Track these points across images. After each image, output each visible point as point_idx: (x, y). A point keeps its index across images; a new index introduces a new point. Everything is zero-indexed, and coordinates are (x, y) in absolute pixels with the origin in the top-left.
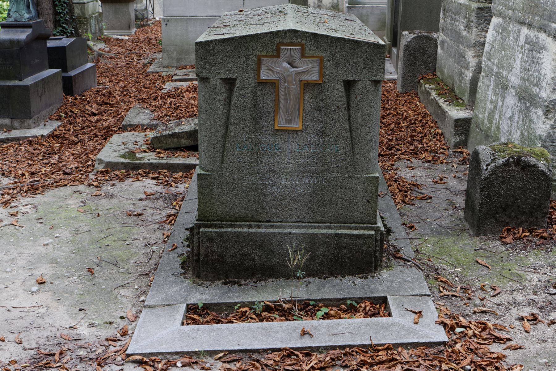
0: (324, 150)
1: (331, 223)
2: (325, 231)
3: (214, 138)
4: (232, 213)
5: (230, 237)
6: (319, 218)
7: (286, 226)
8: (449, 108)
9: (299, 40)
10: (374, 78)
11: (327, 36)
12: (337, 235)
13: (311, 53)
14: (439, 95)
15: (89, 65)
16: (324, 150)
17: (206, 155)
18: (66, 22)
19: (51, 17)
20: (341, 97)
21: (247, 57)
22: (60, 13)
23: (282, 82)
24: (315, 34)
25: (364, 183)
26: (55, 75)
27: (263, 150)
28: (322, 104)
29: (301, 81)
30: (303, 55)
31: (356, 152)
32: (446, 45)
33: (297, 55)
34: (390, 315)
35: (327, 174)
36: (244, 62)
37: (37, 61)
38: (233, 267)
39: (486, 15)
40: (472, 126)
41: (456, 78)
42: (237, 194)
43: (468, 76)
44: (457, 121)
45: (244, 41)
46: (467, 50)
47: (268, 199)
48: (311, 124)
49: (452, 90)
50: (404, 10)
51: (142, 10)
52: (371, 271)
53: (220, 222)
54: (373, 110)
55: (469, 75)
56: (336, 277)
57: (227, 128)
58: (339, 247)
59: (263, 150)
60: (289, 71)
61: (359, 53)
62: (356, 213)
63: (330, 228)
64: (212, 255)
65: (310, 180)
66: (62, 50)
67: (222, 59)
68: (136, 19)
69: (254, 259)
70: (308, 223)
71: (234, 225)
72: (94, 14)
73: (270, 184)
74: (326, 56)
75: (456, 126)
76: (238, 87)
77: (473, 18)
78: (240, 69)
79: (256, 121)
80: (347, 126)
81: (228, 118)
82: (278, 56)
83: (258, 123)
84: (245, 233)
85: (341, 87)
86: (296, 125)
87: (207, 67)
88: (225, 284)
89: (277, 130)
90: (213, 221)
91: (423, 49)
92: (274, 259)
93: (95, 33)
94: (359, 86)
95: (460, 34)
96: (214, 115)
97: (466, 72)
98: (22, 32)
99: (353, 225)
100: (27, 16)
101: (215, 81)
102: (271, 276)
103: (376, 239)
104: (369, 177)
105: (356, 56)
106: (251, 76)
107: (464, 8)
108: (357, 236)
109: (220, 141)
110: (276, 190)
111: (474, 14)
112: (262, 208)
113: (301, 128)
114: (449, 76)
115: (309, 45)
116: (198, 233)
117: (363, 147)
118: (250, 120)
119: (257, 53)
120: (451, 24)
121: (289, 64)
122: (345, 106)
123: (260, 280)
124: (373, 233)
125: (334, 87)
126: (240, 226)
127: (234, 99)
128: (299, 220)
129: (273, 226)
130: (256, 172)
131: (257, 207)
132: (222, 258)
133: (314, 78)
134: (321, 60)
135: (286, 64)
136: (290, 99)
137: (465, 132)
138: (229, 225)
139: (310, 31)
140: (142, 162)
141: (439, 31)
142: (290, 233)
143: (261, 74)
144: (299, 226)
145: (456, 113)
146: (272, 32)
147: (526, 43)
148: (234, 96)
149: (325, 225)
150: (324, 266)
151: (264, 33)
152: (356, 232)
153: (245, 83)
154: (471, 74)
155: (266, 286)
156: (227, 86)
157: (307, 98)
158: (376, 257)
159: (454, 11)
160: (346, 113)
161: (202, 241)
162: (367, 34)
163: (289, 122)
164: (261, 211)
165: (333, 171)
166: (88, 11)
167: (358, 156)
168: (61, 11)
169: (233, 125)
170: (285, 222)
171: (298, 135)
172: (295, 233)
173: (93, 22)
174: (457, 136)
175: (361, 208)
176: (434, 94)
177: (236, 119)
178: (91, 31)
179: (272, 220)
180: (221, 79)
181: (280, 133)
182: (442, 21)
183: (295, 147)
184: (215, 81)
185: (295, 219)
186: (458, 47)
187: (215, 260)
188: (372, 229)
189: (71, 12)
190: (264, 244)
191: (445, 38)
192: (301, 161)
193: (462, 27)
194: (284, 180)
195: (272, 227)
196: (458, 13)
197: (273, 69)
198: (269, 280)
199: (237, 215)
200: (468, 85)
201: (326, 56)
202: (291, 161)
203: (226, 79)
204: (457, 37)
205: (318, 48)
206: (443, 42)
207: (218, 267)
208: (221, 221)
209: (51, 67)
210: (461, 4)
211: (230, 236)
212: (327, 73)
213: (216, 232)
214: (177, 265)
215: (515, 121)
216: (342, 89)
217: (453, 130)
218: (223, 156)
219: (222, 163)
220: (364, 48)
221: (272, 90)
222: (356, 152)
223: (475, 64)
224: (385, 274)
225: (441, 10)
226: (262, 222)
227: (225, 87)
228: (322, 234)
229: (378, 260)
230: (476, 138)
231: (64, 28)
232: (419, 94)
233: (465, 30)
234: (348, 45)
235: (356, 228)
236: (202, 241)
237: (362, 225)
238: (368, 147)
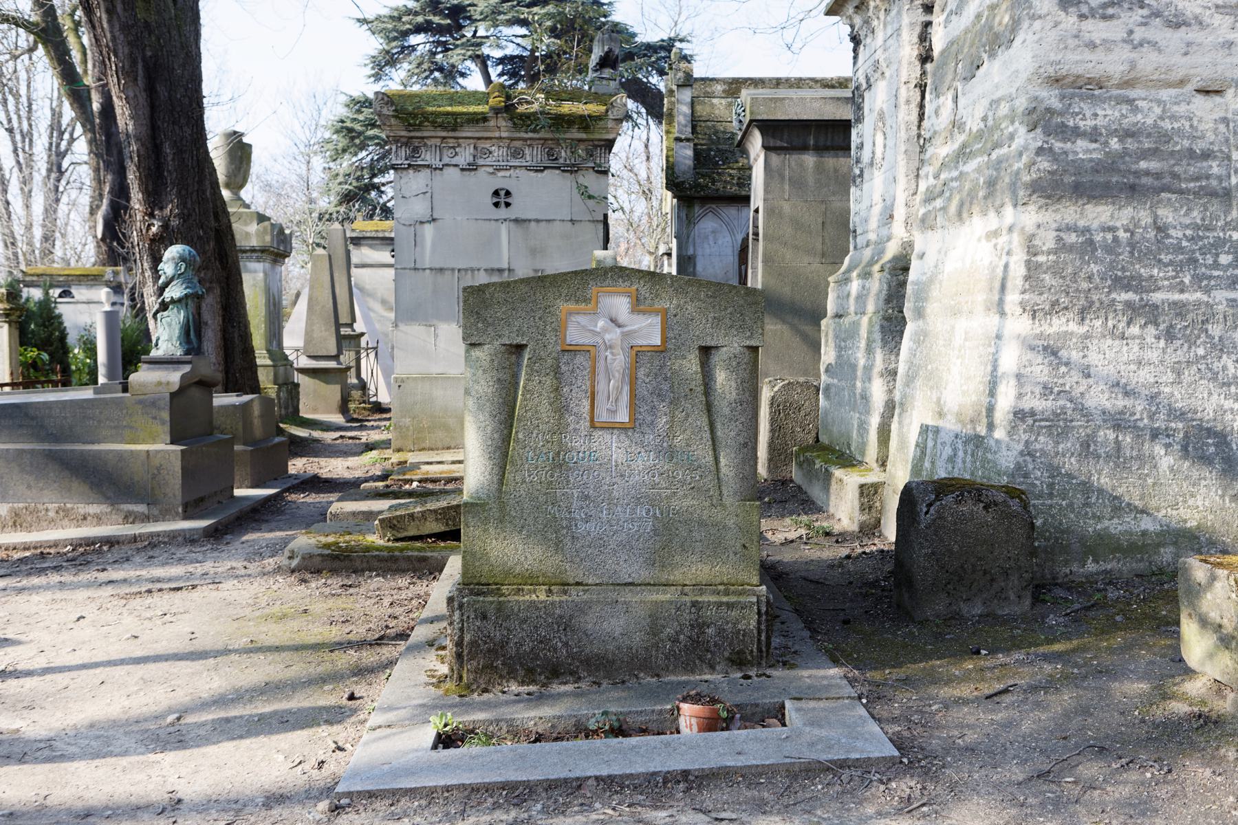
10: (748, 343)
32: (833, 390)
98: (175, 370)
128: (630, 580)
147: (966, 339)
171: (628, 437)
203: (510, 345)
215: (959, 460)
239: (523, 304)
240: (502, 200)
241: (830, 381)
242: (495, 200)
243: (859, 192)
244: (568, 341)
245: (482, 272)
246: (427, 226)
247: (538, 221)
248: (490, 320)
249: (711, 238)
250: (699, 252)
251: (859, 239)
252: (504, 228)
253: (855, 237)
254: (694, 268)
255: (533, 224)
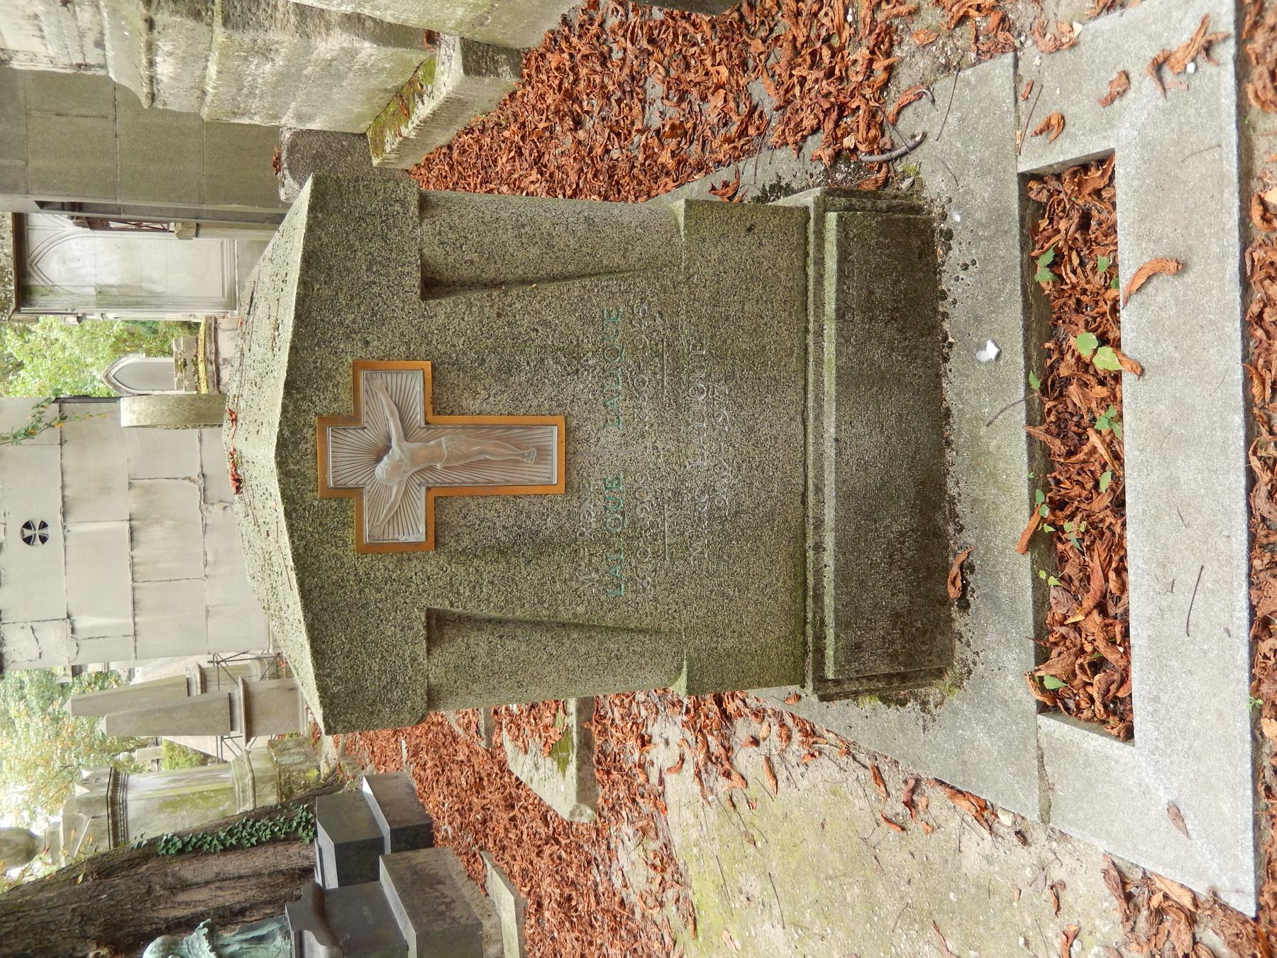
0: (618, 353)
1: (807, 331)
2: (830, 349)
3: (594, 659)
4: (784, 597)
5: (848, 599)
6: (794, 364)
7: (816, 451)
8: (436, 93)
9: (308, 432)
10: (413, 209)
11: (294, 349)
12: (840, 314)
13: (345, 396)
14: (408, 116)
15: (366, 789)
16: (618, 353)
17: (638, 677)
18: (289, 820)
19: (280, 848)
20: (470, 305)
21: (364, 581)
22: (272, 832)
23: (431, 478)
24: (289, 385)
25: (704, 240)
26: (391, 871)
27: (621, 524)
28: (493, 361)
29: (427, 423)
30: (352, 419)
31: (623, 262)
32: (304, 110)
33: (351, 436)
34: (1104, 160)
35: (683, 343)
36: (379, 591)
37: (366, 910)
38: (919, 586)
39: (239, 8)
40: (478, 38)
41: (373, 83)
42: (737, 585)
43: (370, 51)
44: (467, 71)
45: (315, 594)
46: (314, 56)
47: (748, 503)
48: (549, 390)
49: (399, 93)
50: (238, 200)
51: (263, 665)
52: (929, 222)
53: (809, 627)
54: (504, 215)
55: (367, 49)
56: (945, 315)
57: (564, 625)
58: (869, 307)
59: (621, 524)
60: (401, 460)
61: (341, 254)
62: (782, 263)
63: (819, 333)
64: (893, 642)
65: (697, 389)
66: (342, 852)
67: (371, 656)
68: (278, 677)
69: (902, 534)
70: (806, 393)
71: (815, 590)
72: (272, 758)
73: (711, 499)
74: (351, 352)
75: (479, 73)
76: (452, 604)
77: (247, 37)
78: (399, 599)
79: (541, 546)
80: (552, 287)
81: (536, 624)
82: (357, 491)
83: (548, 542)
84: (837, 560)
85: (443, 307)
86: (553, 438)
87: (396, 695)
88: (964, 605)
89: (568, 484)
90: (805, 643)
91: (314, 158)
92: (899, 481)
93: (305, 754)
94: (436, 253)
95: (281, 74)
96: (530, 663)
97: (362, 56)
99: (811, 271)
100: (279, 941)
101: (436, 668)
102: (941, 488)
103: (846, 209)
104: (686, 226)
105: (349, 264)
106: (419, 567)
107: (228, 64)
108: (843, 259)
109: (601, 643)
110: (725, 482)
111: (237, 36)
112: (770, 517)
113: (561, 420)
114: (369, 99)
115: (322, 403)
116: (837, 682)
117: (609, 244)
118: (542, 563)
119: (350, 557)
120: (262, 97)
121: (378, 460)
122: (495, 293)
123: (954, 515)
124: (832, 217)
125: (443, 328)
126: (819, 573)
127: (486, 611)
128: (799, 418)
129: (816, 486)
130: (680, 539)
131: (767, 532)
132: (898, 615)
133: (419, 388)
134: (364, 368)
135: (381, 470)
136: (481, 453)
137: (490, 54)
138: (815, 603)
139: (280, 401)
140: (575, 729)
141: (278, 127)
142: (837, 440)
143: (412, 539)
144: (818, 418)
145: (449, 74)
146: (288, 514)
148: (475, 612)
149: (811, 349)
150: (916, 347)
151: (291, 536)
152: (831, 264)
153: (435, 581)
154: (367, 44)
155: (975, 500)
156: (449, 631)
157: (475, 405)
158: (889, 209)
159: (234, 90)
160: (514, 292)
161: (857, 672)
162: (283, 240)
163: (542, 453)
164: (779, 519)
165: (674, 328)
166: (267, 770)
167: (633, 257)
168: (268, 832)
169: (557, 611)
170: (805, 453)
171: (578, 428)
172: (838, 427)
173: (286, 760)
174: (500, 71)
175: (768, 249)
176: (408, 130)
177: (541, 602)
178: (301, 763)
179: (801, 489)
180: (429, 651)
181: (575, 478)
182: (257, 120)
183: (612, 436)
184: (436, 668)
185: (797, 427)
186: (308, 78)
187: (902, 635)
188: (821, 220)
189: (269, 812)
190: (862, 508)
191: (290, 113)
192: (649, 415)
193: (268, 67)
194: (699, 462)
195: (819, 489)
196: (239, 77)
197: (395, 506)
198: (953, 492)
199: (790, 583)
200: (390, 50)
201: (351, 352)
202: (649, 444)
203: (428, 639)
204: (287, 80)
205: (329, 377)
206: (300, 117)
207: (919, 625)
208: (806, 623)
209: (376, 877)
210: (219, 72)
211: (846, 598)
212: (403, 348)
213: (837, 636)
214: (892, 713)
216: (447, 302)
217: (487, 80)
218: (641, 631)
219: (658, 632)
220: (325, 240)
221: (457, 505)
222: (623, 262)
223: (345, 35)
224: (936, 186)
225: (236, 121)
226: (805, 515)
227: (451, 640)
228: (839, 354)
229: (898, 205)
230: (505, 25)
231: (299, 824)
232: (404, 166)
233: (273, 60)
234: (317, 286)
235: (820, 262)
236: (857, 672)
237: (811, 249)
238: (608, 230)
239: (353, 622)
240: (38, 532)
241: (290, 113)
242: (38, 541)
243: (20, 56)
244: (423, 539)
245: (135, 553)
246: (77, 625)
247: (63, 487)
248: (385, 680)
249: (72, 265)
250: (92, 280)
251: (90, 61)
252: (75, 528)
253: (87, 66)
254: (113, 286)
255: (67, 492)
